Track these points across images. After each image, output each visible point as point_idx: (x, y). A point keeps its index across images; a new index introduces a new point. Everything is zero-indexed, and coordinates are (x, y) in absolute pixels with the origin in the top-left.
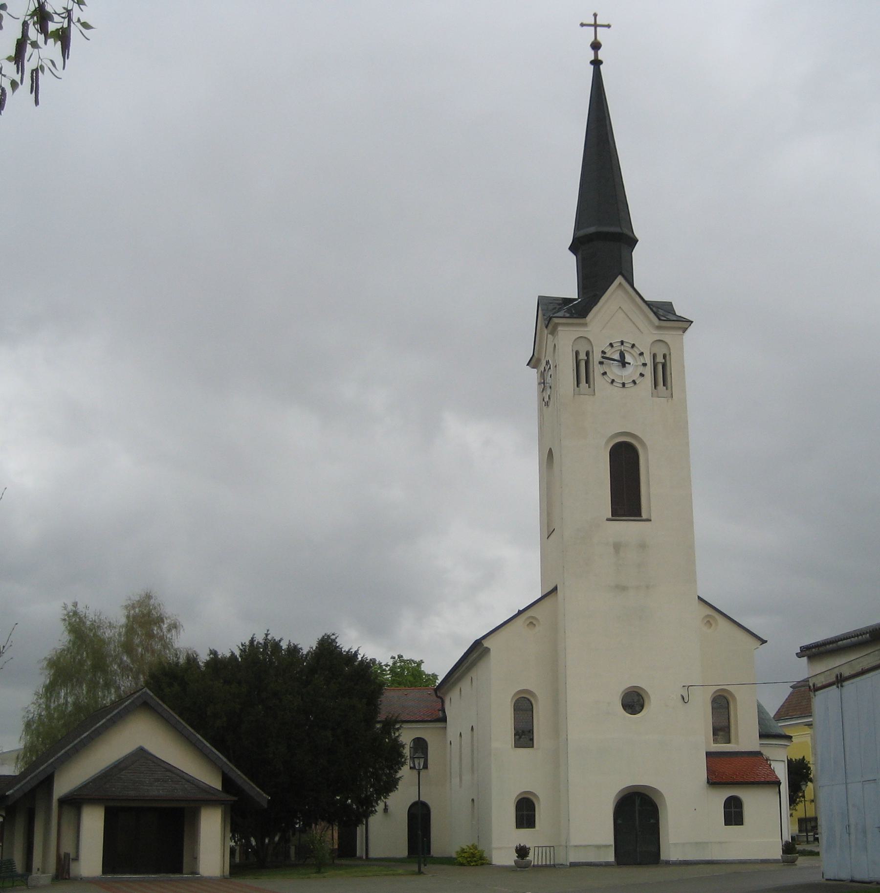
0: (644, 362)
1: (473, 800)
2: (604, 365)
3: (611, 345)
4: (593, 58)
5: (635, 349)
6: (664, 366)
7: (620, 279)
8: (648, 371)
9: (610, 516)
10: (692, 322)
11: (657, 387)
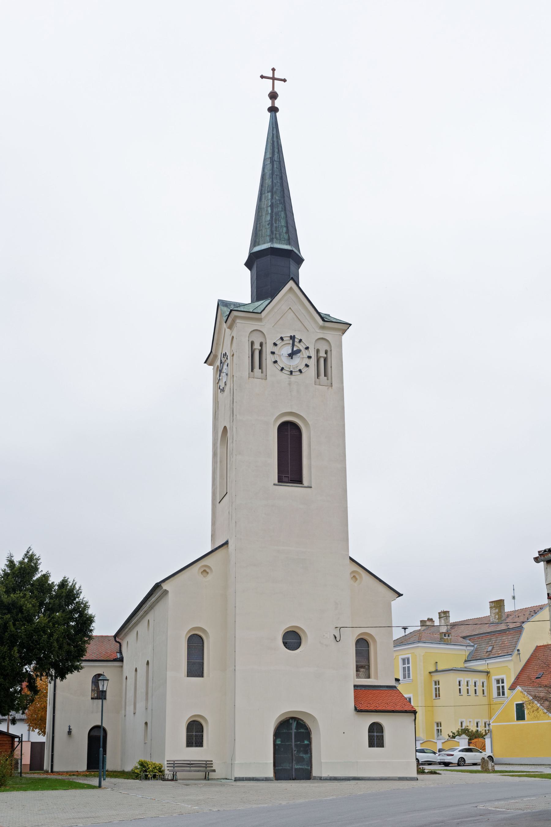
0: (309, 355)
1: (146, 723)
2: (275, 355)
3: (282, 339)
4: (270, 105)
5: (301, 343)
6: (325, 360)
7: (291, 284)
8: (312, 363)
9: (276, 482)
10: (350, 325)
11: (319, 377)
